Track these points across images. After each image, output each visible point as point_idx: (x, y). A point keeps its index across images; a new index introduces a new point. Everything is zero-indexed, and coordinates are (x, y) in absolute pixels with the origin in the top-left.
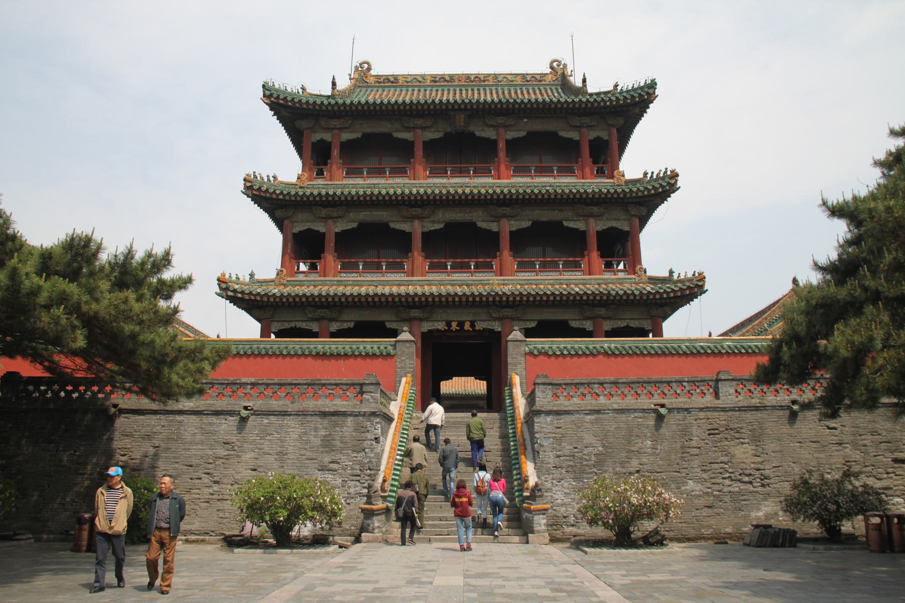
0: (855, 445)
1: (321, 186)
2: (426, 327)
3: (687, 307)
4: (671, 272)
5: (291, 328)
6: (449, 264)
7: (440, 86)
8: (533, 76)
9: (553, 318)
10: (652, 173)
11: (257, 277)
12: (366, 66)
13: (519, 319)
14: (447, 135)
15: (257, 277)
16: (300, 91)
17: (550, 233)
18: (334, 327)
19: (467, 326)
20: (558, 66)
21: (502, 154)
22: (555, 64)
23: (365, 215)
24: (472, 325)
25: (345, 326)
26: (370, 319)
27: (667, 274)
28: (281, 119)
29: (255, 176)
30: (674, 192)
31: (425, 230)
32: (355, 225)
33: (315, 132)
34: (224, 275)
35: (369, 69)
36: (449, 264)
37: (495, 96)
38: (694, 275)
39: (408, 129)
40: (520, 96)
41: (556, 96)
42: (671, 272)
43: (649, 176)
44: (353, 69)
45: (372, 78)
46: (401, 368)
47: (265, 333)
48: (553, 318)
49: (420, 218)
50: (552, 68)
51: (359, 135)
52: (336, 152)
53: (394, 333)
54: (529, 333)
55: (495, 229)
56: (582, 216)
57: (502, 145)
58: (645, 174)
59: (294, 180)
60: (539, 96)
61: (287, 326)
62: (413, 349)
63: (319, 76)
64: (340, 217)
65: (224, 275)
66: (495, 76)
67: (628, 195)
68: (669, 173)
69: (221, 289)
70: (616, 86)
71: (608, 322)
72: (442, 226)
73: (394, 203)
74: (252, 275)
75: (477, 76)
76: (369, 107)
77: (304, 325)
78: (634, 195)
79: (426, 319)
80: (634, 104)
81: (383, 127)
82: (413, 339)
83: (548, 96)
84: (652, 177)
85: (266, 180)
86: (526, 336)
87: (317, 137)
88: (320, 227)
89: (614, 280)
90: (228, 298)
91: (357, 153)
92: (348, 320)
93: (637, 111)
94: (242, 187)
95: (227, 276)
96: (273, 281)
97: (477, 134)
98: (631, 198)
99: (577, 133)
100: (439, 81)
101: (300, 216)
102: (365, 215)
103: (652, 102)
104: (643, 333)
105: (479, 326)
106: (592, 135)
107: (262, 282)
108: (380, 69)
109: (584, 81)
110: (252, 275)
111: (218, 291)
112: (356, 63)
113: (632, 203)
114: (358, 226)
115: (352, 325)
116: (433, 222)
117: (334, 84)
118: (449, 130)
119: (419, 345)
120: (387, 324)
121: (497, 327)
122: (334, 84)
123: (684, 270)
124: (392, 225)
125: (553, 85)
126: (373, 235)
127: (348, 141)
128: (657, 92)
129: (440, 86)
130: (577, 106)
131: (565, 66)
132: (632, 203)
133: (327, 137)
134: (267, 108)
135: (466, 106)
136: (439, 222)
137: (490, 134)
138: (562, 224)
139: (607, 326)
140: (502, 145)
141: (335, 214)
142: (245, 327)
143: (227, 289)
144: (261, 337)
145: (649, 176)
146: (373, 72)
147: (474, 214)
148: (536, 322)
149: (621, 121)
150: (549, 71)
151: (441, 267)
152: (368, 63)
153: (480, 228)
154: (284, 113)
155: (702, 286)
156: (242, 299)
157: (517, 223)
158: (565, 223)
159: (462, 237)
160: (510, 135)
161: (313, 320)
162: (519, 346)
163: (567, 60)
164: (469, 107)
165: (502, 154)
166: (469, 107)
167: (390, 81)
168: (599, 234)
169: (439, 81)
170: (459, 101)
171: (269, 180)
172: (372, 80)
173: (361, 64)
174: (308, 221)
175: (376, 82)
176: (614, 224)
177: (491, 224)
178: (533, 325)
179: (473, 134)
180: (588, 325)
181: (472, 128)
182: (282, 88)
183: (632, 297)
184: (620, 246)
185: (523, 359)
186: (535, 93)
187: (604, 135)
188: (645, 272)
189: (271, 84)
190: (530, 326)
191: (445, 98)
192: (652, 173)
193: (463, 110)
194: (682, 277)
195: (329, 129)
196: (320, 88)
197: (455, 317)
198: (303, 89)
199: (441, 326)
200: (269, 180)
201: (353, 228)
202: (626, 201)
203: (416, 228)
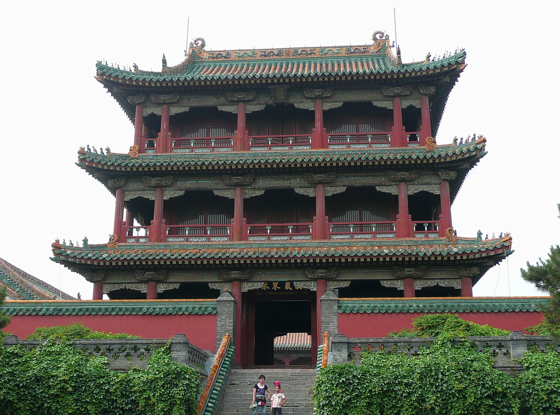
0: (537, 390)
1: (152, 157)
2: (246, 287)
3: (496, 267)
4: (480, 234)
5: (122, 289)
6: (269, 228)
7: (268, 60)
8: (357, 48)
9: (365, 279)
10: (462, 139)
11: (89, 243)
12: (200, 42)
13: (333, 280)
14: (268, 107)
15: (89, 243)
16: (133, 69)
17: (361, 198)
18: (161, 288)
19: (287, 286)
20: (381, 37)
21: (318, 124)
22: (378, 36)
23: (191, 184)
24: (292, 285)
25: (171, 287)
26: (193, 281)
27: (475, 236)
28: (116, 96)
29: (89, 149)
30: (482, 157)
31: (247, 196)
32: (182, 193)
33: (146, 107)
34: (58, 241)
35: (203, 45)
36: (269, 228)
37: (366, 68)
38: (501, 236)
39: (232, 103)
40: (383, 68)
41: (375, 67)
42: (480, 234)
43: (458, 142)
44: (189, 46)
45: (205, 54)
46: (222, 326)
47: (98, 295)
48: (365, 279)
49: (241, 185)
50: (375, 39)
51: (187, 109)
52: (164, 125)
53: (215, 294)
54: (343, 293)
55: (312, 195)
56: (394, 181)
57: (319, 116)
58: (456, 140)
59: (126, 151)
60: (360, 67)
61: (117, 288)
62: (230, 309)
63: (154, 53)
64: (168, 186)
65: (58, 241)
66: (322, 49)
67: (437, 161)
68: (477, 139)
69: (55, 254)
70: (429, 57)
71: (418, 282)
72: (262, 192)
73: (217, 172)
74: (85, 241)
75: (304, 50)
76: (352, 78)
77: (133, 287)
78: (442, 160)
79: (247, 281)
80: (445, 74)
81: (209, 102)
82: (232, 299)
83: (369, 68)
84: (461, 142)
85: (99, 152)
86: (340, 296)
87: (148, 111)
88: (150, 196)
89: (425, 244)
90: (62, 262)
91: (183, 125)
92: (174, 282)
93: (447, 79)
94: (77, 160)
95: (61, 243)
96: (105, 246)
97: (296, 105)
98: (440, 163)
99: (312, 104)
100: (268, 55)
101: (132, 185)
102: (191, 184)
103: (462, 71)
104: (455, 292)
105: (299, 286)
106: (406, 104)
107: (94, 248)
108: (213, 45)
109: (399, 53)
110: (85, 241)
111: (53, 256)
112: (189, 42)
113: (441, 168)
114: (185, 194)
115: (177, 286)
116: (254, 189)
117: (164, 62)
118: (270, 102)
119: (239, 304)
120: (210, 284)
121: (313, 287)
122: (164, 62)
123: (492, 232)
124: (216, 193)
125: (376, 56)
126: (194, 205)
127: (177, 115)
128: (466, 61)
129: (268, 60)
130: (389, 77)
131: (387, 38)
132: (441, 168)
133: (157, 111)
134: (102, 85)
135: (284, 80)
136: (259, 189)
137: (308, 105)
138: (376, 189)
139: (419, 285)
140: (319, 116)
141: (163, 183)
142: (79, 288)
143: (60, 254)
144: (93, 299)
145: (458, 142)
146: (207, 48)
147: (292, 181)
148: (349, 282)
149: (432, 90)
150: (371, 42)
151: (261, 231)
152: (199, 39)
153: (298, 194)
154: (115, 90)
155: (509, 247)
156: (80, 264)
157: (332, 189)
158: (378, 189)
159: (279, 206)
160: (327, 106)
161: (141, 282)
162: (330, 311)
163: (389, 31)
164: (287, 81)
165: (318, 124)
166: (287, 81)
167: (217, 56)
168: (411, 198)
169: (267, 54)
170: (319, 74)
171: (102, 152)
172: (205, 56)
173: (195, 41)
174: (139, 190)
175: (261, 56)
176: (426, 188)
177: (308, 190)
178: (346, 284)
179: (293, 105)
180: (399, 285)
181: (291, 101)
182: (115, 67)
183: (439, 258)
184: (430, 211)
185: (335, 317)
186: (363, 65)
187: (416, 103)
188: (456, 234)
189: (104, 63)
190: (344, 286)
191: (306, 73)
192: (462, 139)
193: (120, 84)
194: (490, 238)
195: (159, 104)
196: (152, 65)
197: (276, 278)
198: (136, 67)
199: (258, 286)
200: (102, 152)
201: (180, 196)
202: (436, 166)
203: (237, 196)
